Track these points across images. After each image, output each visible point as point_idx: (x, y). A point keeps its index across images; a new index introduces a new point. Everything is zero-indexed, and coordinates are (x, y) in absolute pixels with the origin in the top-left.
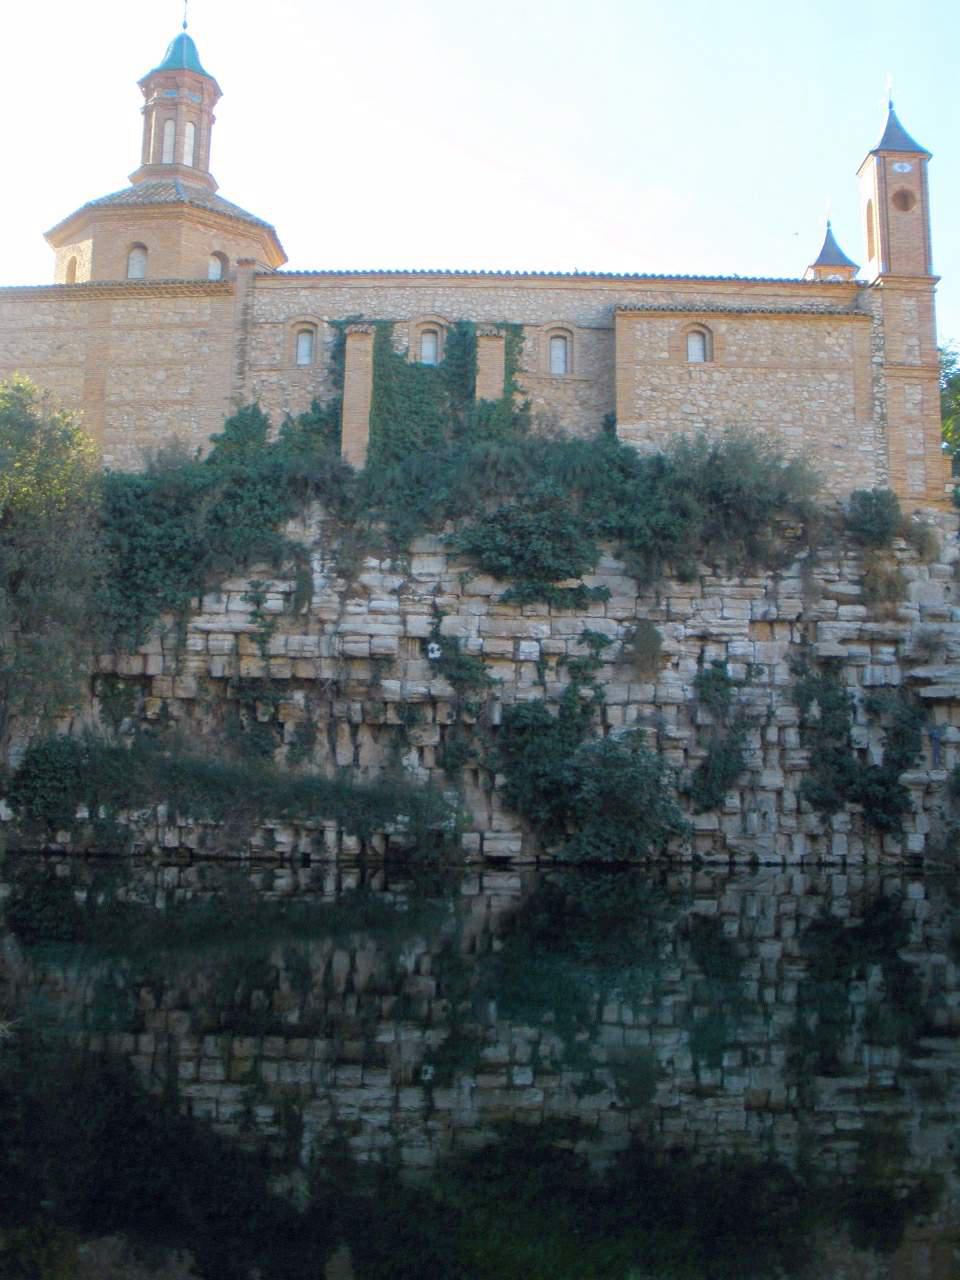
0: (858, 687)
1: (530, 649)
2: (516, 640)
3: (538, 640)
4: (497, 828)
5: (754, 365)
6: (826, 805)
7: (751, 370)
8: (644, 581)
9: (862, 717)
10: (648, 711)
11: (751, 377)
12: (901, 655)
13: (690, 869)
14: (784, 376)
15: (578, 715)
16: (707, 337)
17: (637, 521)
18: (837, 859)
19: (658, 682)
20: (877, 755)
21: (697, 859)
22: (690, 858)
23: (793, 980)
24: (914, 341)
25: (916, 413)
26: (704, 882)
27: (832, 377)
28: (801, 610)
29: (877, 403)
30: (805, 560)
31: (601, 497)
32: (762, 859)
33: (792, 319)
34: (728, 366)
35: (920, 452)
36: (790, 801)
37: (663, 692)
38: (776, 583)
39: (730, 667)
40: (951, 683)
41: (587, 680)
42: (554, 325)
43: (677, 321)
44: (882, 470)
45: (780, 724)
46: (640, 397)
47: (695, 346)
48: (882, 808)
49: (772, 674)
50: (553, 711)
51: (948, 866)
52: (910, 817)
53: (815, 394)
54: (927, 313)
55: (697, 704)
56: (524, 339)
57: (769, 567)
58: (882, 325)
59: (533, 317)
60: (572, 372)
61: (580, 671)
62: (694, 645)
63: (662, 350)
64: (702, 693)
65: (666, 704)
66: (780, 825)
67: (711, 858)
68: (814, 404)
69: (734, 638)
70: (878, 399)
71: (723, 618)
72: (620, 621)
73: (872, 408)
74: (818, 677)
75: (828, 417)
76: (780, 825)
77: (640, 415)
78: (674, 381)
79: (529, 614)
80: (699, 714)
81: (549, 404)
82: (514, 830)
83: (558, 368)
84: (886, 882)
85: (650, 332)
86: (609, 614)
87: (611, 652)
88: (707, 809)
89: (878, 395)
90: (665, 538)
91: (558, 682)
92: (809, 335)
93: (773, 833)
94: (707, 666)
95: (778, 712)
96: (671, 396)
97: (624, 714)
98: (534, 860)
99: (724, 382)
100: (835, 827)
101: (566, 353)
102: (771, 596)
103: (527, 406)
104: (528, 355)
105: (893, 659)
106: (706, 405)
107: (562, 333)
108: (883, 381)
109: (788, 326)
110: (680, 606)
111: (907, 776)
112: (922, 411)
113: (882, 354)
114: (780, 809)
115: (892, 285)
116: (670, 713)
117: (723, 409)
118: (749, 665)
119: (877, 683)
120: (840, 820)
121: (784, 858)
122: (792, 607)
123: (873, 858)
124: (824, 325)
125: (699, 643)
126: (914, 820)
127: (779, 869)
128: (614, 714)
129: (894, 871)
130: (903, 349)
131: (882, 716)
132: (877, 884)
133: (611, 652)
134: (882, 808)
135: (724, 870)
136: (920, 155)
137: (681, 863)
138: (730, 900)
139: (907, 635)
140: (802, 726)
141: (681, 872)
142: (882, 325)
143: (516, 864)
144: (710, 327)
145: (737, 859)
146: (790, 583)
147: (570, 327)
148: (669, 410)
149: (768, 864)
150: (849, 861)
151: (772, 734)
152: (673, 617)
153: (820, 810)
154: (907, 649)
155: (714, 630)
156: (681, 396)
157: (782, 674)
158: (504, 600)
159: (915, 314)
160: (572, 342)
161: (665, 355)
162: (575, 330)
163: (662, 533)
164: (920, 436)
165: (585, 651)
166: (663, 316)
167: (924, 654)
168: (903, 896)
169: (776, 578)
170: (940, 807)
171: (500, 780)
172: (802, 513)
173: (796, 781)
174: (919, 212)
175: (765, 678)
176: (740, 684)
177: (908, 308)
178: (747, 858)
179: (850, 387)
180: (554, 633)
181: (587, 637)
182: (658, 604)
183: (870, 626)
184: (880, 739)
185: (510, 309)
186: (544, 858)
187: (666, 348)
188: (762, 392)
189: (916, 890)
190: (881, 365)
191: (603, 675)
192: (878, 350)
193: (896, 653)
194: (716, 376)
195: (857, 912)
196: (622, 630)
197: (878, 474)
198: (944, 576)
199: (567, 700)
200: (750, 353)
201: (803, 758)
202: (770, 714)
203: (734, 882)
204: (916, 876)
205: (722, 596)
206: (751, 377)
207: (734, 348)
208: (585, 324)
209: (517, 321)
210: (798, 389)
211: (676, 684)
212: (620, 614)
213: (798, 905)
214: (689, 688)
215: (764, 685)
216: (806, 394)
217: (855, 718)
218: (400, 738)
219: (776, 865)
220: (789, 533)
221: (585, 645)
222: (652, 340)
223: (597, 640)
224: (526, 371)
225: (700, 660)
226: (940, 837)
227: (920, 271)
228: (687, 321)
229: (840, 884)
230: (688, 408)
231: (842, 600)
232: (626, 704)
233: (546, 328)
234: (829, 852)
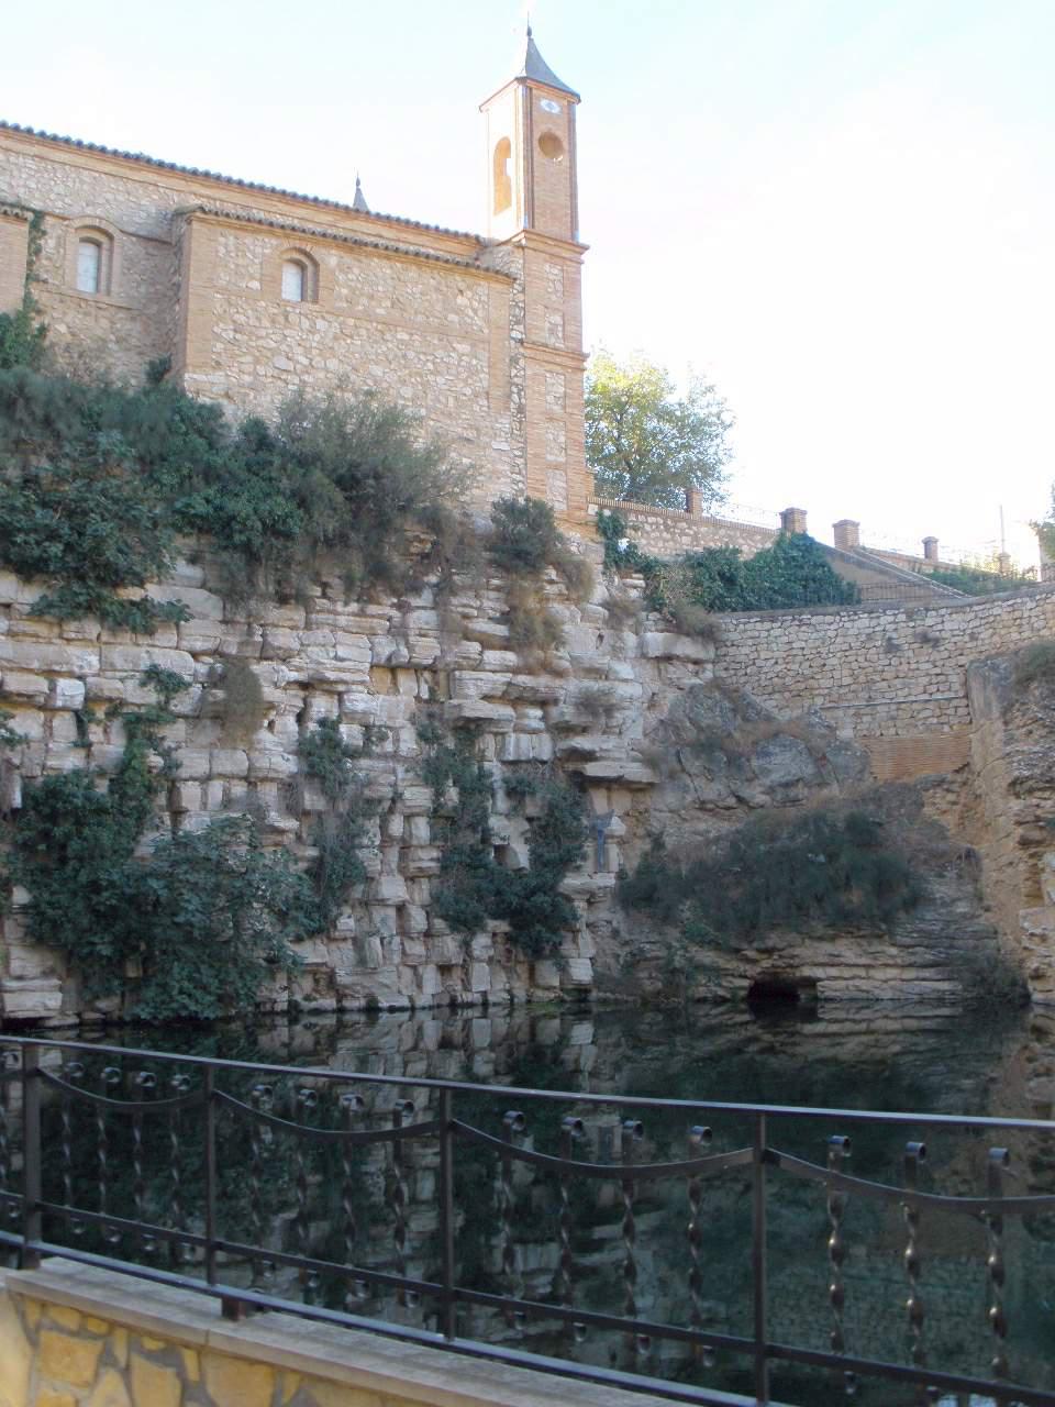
0: (495, 763)
1: (70, 691)
2: (50, 674)
3: (81, 678)
4: (18, 972)
5: (368, 316)
6: (464, 924)
7: (365, 324)
8: (232, 595)
9: (502, 803)
10: (239, 789)
11: (363, 332)
12: (552, 722)
13: (285, 1021)
14: (406, 337)
15: (138, 788)
16: (310, 269)
17: (240, 506)
18: (477, 998)
19: (251, 747)
20: (521, 855)
21: (293, 1005)
22: (285, 1006)
23: (427, 1168)
24: (557, 319)
25: (557, 408)
26: (304, 1039)
27: (464, 348)
28: (438, 653)
29: (515, 390)
30: (436, 585)
31: (178, 470)
32: (384, 1004)
33: (419, 266)
34: (336, 313)
35: (562, 459)
36: (418, 920)
37: (262, 763)
38: (404, 614)
39: (343, 728)
40: (614, 760)
41: (154, 742)
42: (88, 222)
43: (274, 242)
44: (519, 477)
45: (408, 811)
46: (218, 337)
47: (290, 282)
48: (534, 923)
49: (397, 741)
50: (102, 787)
51: (631, 999)
52: (570, 935)
53: (442, 368)
54: (571, 286)
55: (301, 780)
56: (44, 233)
57: (395, 593)
58: (523, 291)
59: (60, 204)
60: (108, 292)
61: (140, 727)
62: (296, 696)
63: (252, 278)
64: (312, 766)
65: (265, 780)
66: (404, 953)
67: (313, 1005)
68: (440, 380)
69: (354, 687)
70: (517, 385)
71: (336, 658)
72: (195, 655)
73: (509, 396)
74: (452, 741)
75: (456, 399)
76: (404, 953)
77: (218, 363)
78: (266, 323)
79: (73, 635)
80: (307, 796)
81: (73, 334)
82: (46, 974)
83: (86, 284)
84: (541, 1024)
85: (237, 249)
86: (184, 644)
87: (188, 700)
88: (313, 934)
89: (516, 380)
90: (277, 534)
91: (110, 745)
92: (437, 290)
93: (396, 968)
94: (312, 726)
95: (407, 795)
96: (260, 342)
97: (205, 793)
98: (77, 1021)
99: (331, 335)
100: (476, 953)
101: (99, 269)
102: (398, 632)
103: (43, 330)
104: (49, 259)
105: (542, 725)
106: (305, 361)
108: (522, 362)
109: (413, 273)
110: (283, 638)
111: (571, 882)
112: (564, 407)
113: (521, 328)
114: (404, 932)
115: (532, 245)
116: (269, 794)
117: (327, 370)
118: (368, 727)
119: (523, 758)
120: (481, 943)
121: (411, 998)
122: (427, 650)
123: (521, 995)
124: (458, 280)
125: (302, 694)
126: (575, 941)
127: (406, 1015)
128: (190, 794)
129: (552, 1009)
130: (544, 326)
131: (528, 800)
132: (526, 1029)
133: (188, 700)
134: (534, 923)
135: (330, 1021)
136: (571, 98)
137: (273, 1013)
138: (341, 1065)
139: (561, 694)
140: (435, 814)
141: (274, 1027)
142: (523, 291)
143: (55, 1029)
144: (317, 257)
145: (347, 1003)
146: (422, 616)
147: (111, 230)
148: (257, 361)
149: (392, 1010)
150: (491, 999)
151: (397, 826)
152: (271, 653)
153: (459, 931)
154: (566, 712)
155: (331, 675)
156: (273, 345)
157: (408, 742)
158: (38, 612)
159: (559, 287)
160: (111, 250)
161: (255, 285)
162: (117, 234)
163: (275, 529)
164: (562, 439)
165: (151, 696)
166: (255, 231)
167: (584, 720)
168: (564, 1039)
169: (402, 607)
170: (609, 922)
172: (434, 521)
173: (423, 892)
174: (566, 163)
175: (389, 747)
176: (354, 754)
177: (551, 277)
178: (362, 1003)
179: (485, 364)
180: (106, 667)
181: (153, 675)
182: (250, 633)
183: (522, 679)
184: (523, 834)
185: (25, 186)
186: (90, 1016)
187: (258, 276)
188: (377, 354)
189: (583, 1033)
190: (521, 342)
191: (174, 733)
192: (518, 323)
193: (544, 718)
194: (321, 324)
195: (501, 1069)
196: (202, 669)
197: (516, 482)
198: (596, 621)
199: (124, 774)
200: (364, 300)
201: (432, 860)
202: (396, 798)
203: (346, 1037)
204: (582, 1014)
205: (335, 627)
206: (363, 332)
207: (345, 291)
208: (132, 229)
209: (36, 205)
210: (422, 357)
211: (276, 749)
212: (199, 645)
213: (429, 1065)
214: (290, 757)
215: (384, 756)
216: (430, 366)
217: (494, 804)
219: (402, 1009)
220: (415, 548)
221: (151, 686)
222: (240, 261)
223: (164, 681)
224: (45, 282)
225: (301, 718)
226: (611, 961)
227: (566, 234)
228: (286, 244)
229: (482, 1032)
230: (282, 363)
231: (487, 643)
232: (206, 779)
233: (77, 223)
234: (467, 987)
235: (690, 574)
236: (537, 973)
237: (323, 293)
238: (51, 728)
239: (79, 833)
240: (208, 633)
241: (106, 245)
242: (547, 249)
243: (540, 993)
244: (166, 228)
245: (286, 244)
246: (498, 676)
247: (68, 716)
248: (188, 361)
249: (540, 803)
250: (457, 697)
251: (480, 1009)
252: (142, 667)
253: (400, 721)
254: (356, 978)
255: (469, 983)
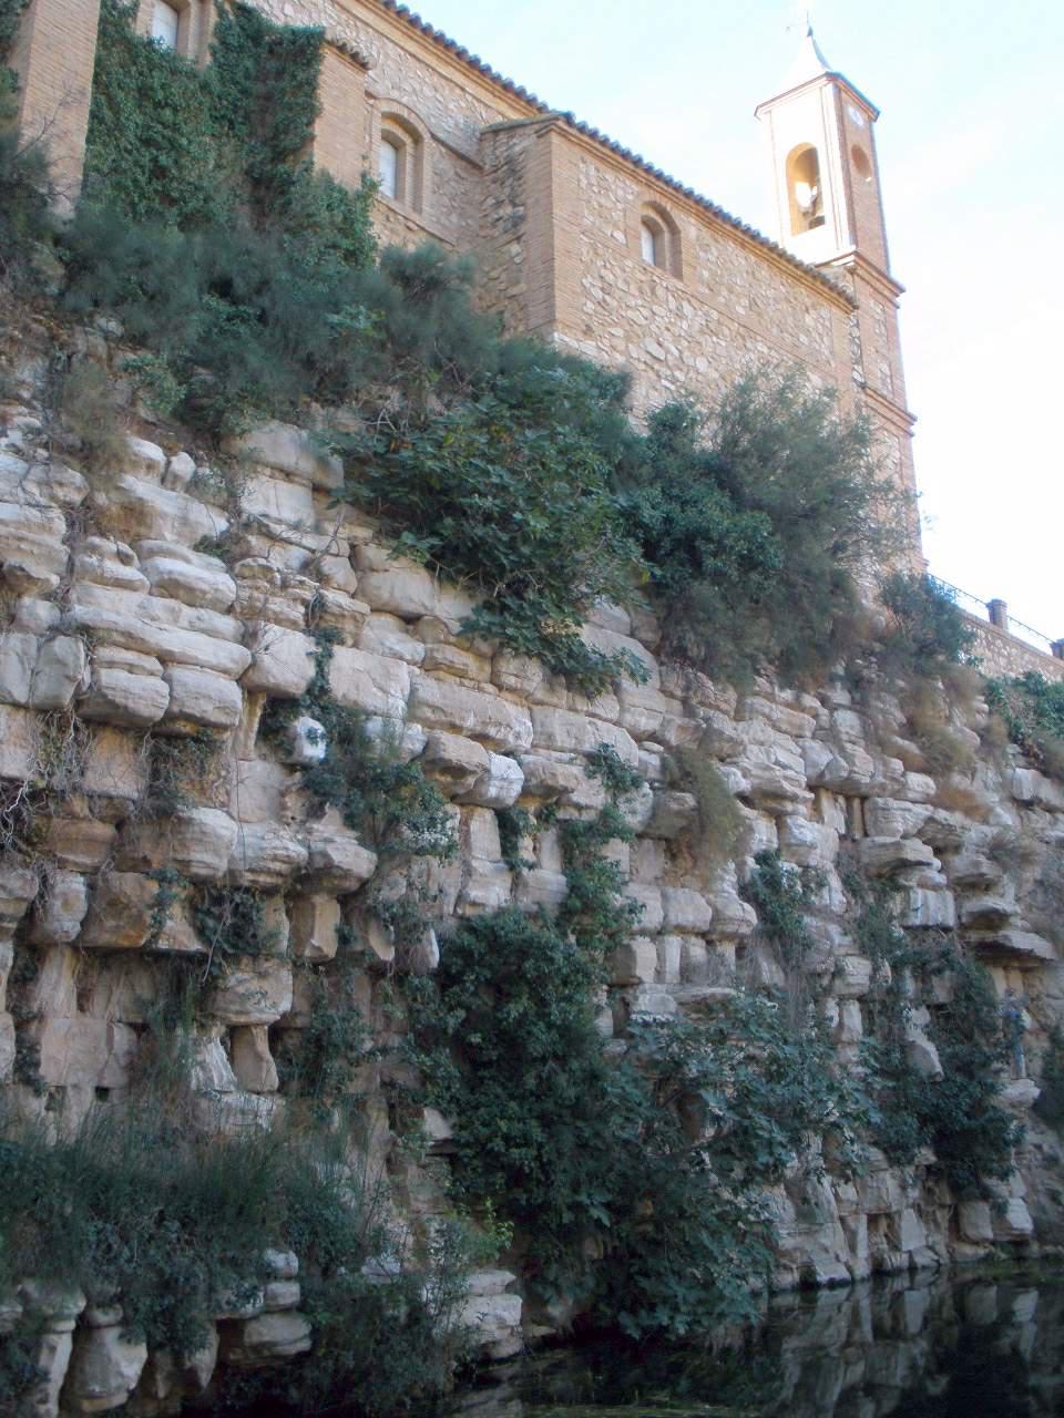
10: (698, 950)
32: (822, 1277)
42: (396, 109)
78: (633, 289)
86: (628, 717)
107: (399, 132)
136: (872, 113)
142: (857, 325)
147: (421, 128)
162: (427, 136)
168: (1007, 1317)
170: (1039, 1147)
171: (435, 1125)
191: (617, 852)
206: (727, 332)
218: (182, 990)
228: (650, 196)
233: (385, 107)
235: (1031, 702)
236: (964, 1222)
237: (686, 270)
238: (468, 831)
239: (543, 1015)
240: (655, 707)
241: (409, 148)
242: (873, 282)
243: (968, 1250)
244: (476, 147)
245: (650, 196)
246: (918, 809)
247: (489, 815)
248: (558, 316)
249: (948, 984)
250: (881, 832)
251: (906, 1275)
252: (587, 747)
253: (830, 866)
254: (799, 1239)
255: (898, 1238)
